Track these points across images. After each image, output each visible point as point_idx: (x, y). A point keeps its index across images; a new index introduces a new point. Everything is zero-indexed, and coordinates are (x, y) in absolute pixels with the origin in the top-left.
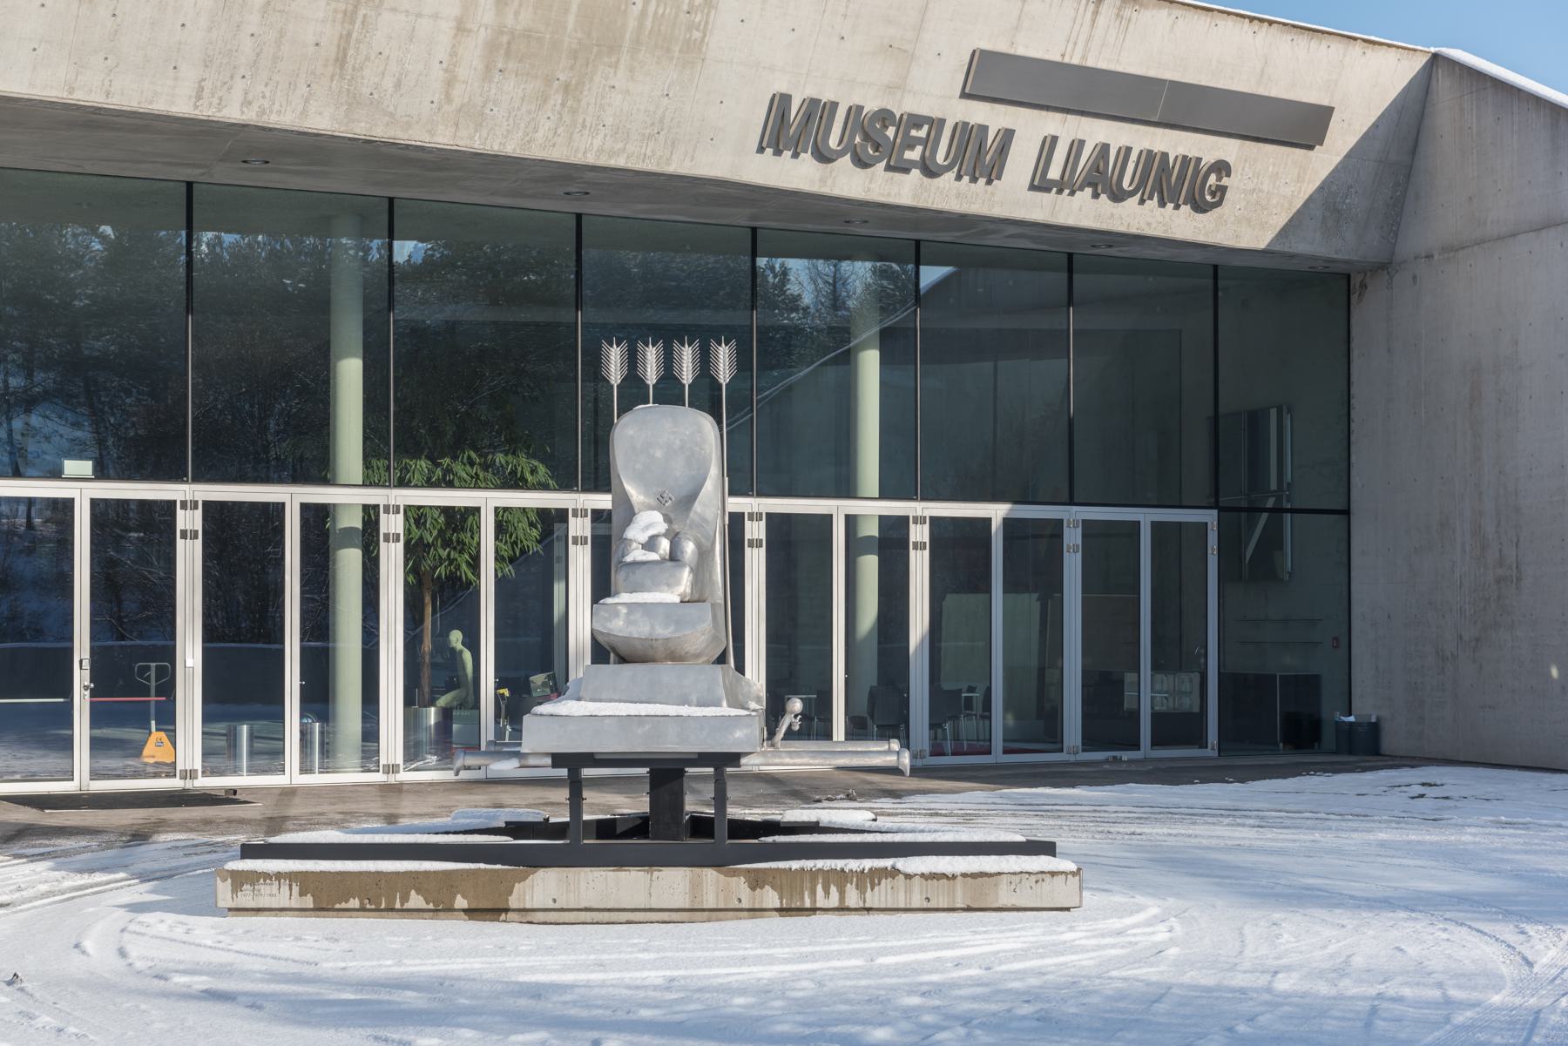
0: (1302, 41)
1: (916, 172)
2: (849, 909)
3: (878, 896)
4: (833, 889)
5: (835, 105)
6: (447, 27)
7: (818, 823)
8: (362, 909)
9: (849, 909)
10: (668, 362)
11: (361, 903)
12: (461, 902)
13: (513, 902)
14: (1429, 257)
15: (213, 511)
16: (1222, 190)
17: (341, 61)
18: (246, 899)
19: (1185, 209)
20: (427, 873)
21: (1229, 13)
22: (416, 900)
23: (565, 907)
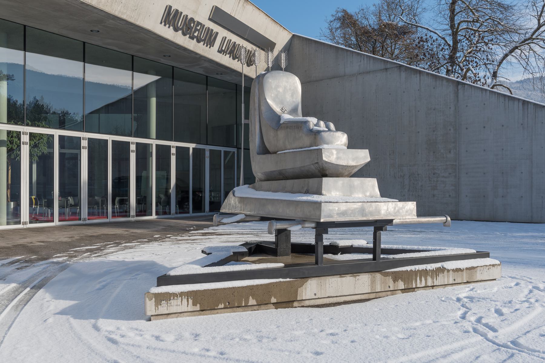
2: (428, 287)
3: (441, 279)
4: (423, 279)
7: (352, 246)
8: (225, 308)
9: (428, 287)
11: (225, 305)
12: (274, 300)
15: (211, 151)
18: (163, 309)
21: (263, 12)
22: (252, 302)
23: (320, 297)
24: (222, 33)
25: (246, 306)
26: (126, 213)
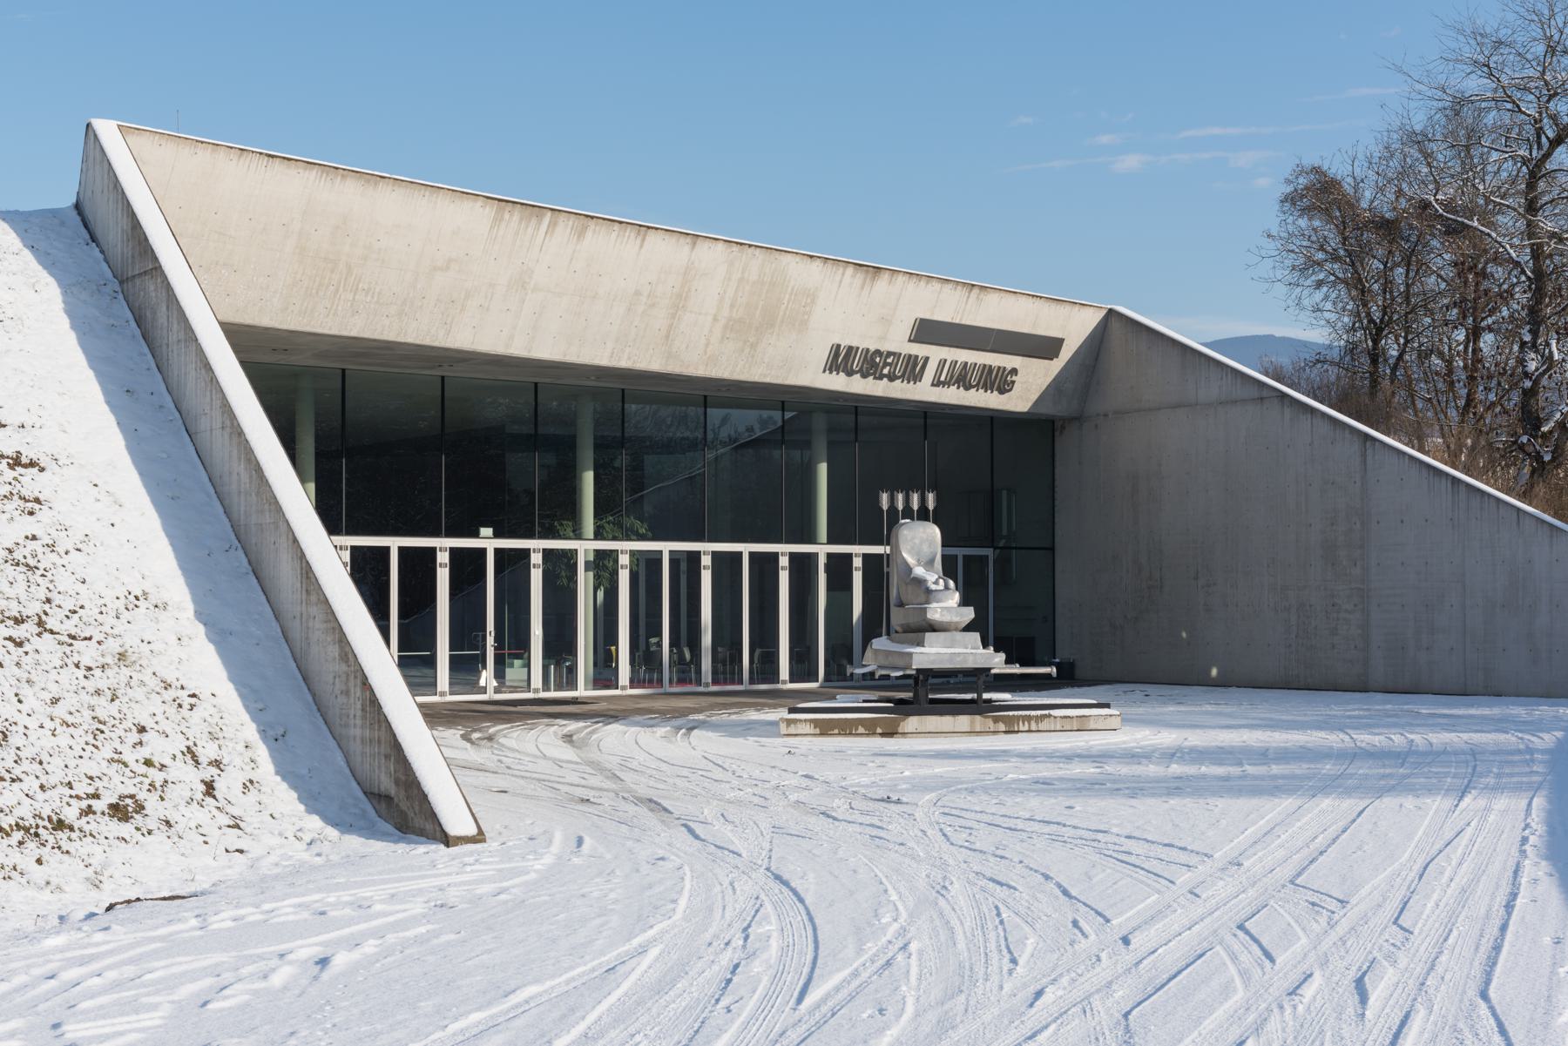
0: (1053, 305)
1: (885, 379)
3: (1043, 725)
5: (858, 348)
6: (710, 318)
8: (839, 734)
10: (907, 500)
12: (879, 730)
13: (900, 730)
14: (1106, 415)
15: (454, 552)
16: (1013, 382)
17: (667, 337)
19: (995, 393)
20: (865, 719)
22: (861, 730)
24: (936, 354)
25: (851, 734)
26: (773, 676)
